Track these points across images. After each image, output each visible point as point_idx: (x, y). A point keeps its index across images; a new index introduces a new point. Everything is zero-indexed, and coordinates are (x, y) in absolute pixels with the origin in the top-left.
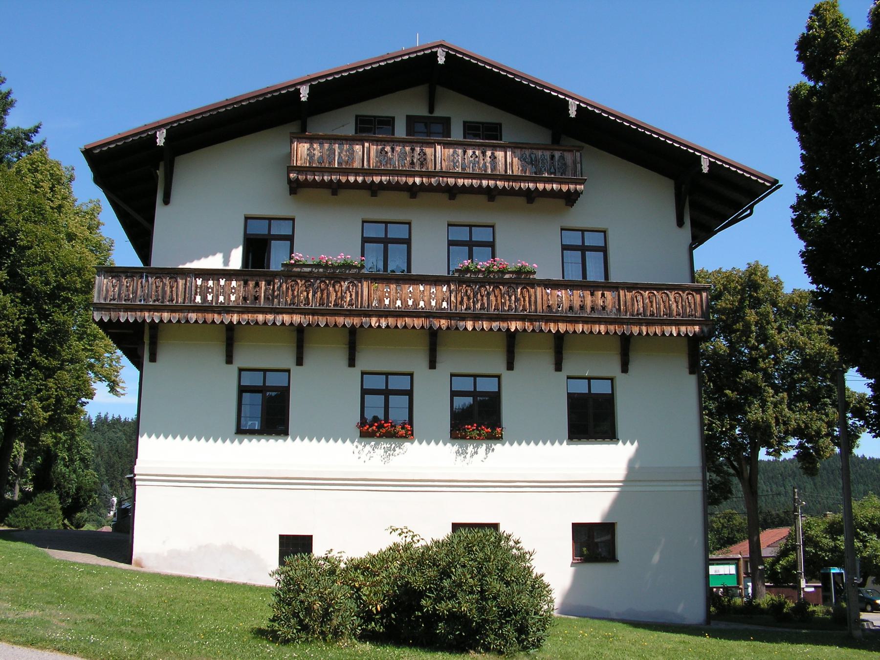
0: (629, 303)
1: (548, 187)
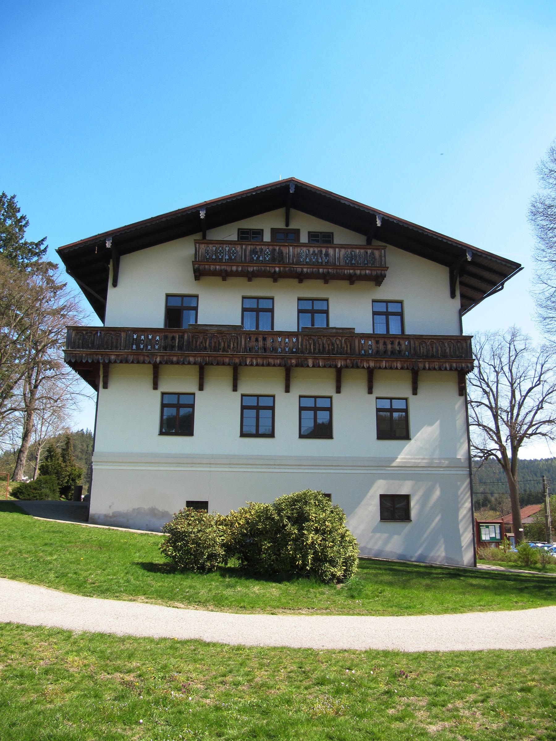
1: (363, 272)
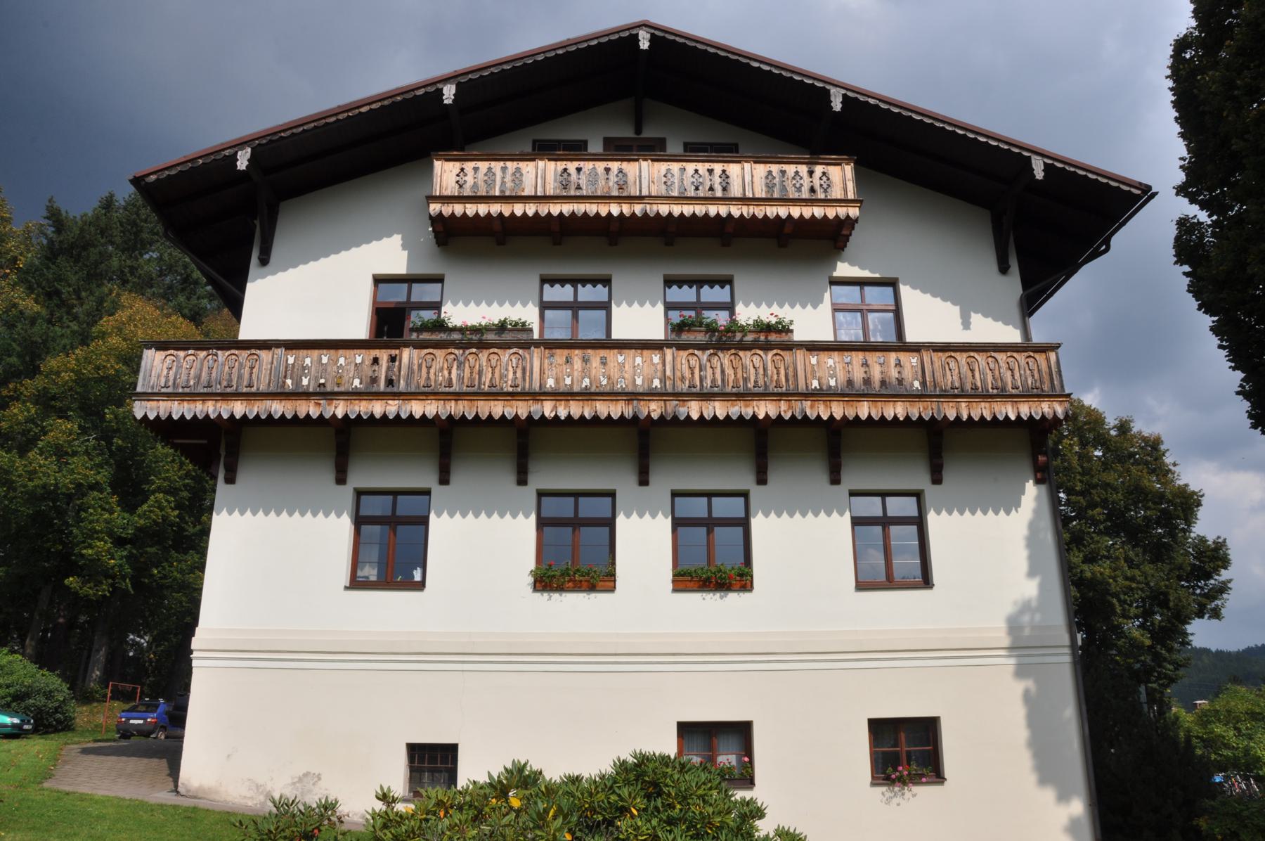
0: (938, 374)
